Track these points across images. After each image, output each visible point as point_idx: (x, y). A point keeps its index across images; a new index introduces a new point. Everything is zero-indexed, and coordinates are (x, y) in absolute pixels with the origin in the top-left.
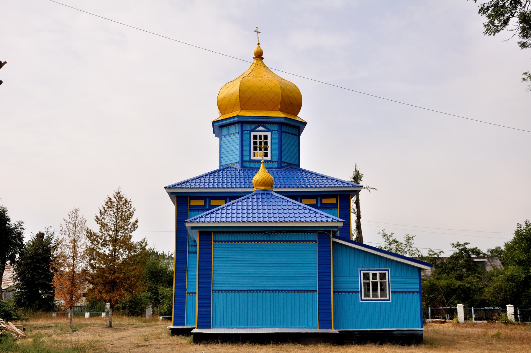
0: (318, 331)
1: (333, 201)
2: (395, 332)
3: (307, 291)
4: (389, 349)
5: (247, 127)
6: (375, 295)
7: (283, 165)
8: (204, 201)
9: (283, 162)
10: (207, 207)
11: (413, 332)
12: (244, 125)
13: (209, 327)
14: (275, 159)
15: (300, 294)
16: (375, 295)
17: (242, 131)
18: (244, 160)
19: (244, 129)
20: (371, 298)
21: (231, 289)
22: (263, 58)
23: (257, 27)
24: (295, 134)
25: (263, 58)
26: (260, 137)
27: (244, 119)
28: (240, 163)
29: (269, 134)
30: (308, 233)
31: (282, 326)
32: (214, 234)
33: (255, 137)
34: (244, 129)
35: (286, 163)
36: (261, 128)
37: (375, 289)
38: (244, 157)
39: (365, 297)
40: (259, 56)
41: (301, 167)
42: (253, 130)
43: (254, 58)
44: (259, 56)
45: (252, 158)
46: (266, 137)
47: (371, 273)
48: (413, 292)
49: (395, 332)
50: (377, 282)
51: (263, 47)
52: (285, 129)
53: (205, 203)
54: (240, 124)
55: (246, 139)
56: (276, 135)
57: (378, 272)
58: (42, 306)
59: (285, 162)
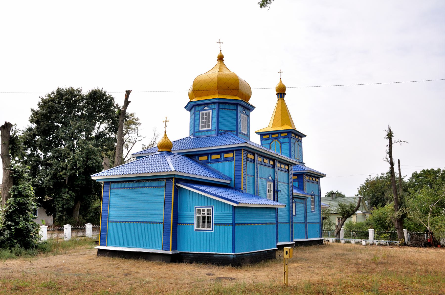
0: (160, 251)
1: (231, 155)
2: (215, 255)
3: (158, 222)
4: (273, 269)
5: (198, 108)
6: (204, 227)
7: (220, 132)
8: (207, 157)
9: (220, 130)
10: (210, 161)
11: (227, 256)
12: (220, 105)
13: (105, 245)
14: (215, 127)
15: (154, 225)
16: (204, 227)
17: (219, 108)
18: (219, 129)
19: (220, 107)
20: (206, 229)
21: (118, 220)
22: (223, 60)
23: (219, 40)
24: (234, 109)
25: (223, 60)
26: (206, 113)
27: (198, 103)
28: (216, 130)
29: (211, 111)
30: (159, 180)
31: (129, 246)
32: (111, 183)
33: (203, 114)
34: (220, 107)
35: (223, 130)
36: (206, 108)
37: (204, 222)
38: (220, 127)
39: (197, 228)
40: (221, 58)
41: (188, 135)
42: (202, 110)
43: (217, 60)
44: (221, 58)
45: (201, 129)
46: (209, 114)
47: (202, 209)
48: (228, 224)
49: (215, 255)
50: (205, 216)
51: (224, 53)
52: (221, 106)
53: (208, 158)
54: (217, 104)
55: (197, 117)
56: (215, 111)
57: (206, 209)
58: (12, 228)
59: (221, 130)
